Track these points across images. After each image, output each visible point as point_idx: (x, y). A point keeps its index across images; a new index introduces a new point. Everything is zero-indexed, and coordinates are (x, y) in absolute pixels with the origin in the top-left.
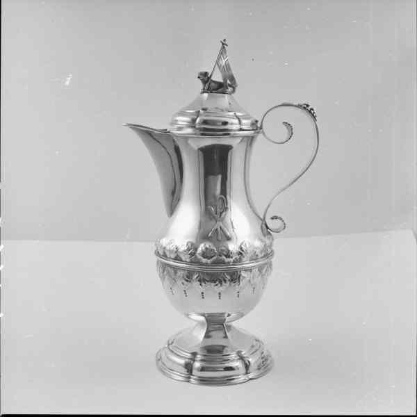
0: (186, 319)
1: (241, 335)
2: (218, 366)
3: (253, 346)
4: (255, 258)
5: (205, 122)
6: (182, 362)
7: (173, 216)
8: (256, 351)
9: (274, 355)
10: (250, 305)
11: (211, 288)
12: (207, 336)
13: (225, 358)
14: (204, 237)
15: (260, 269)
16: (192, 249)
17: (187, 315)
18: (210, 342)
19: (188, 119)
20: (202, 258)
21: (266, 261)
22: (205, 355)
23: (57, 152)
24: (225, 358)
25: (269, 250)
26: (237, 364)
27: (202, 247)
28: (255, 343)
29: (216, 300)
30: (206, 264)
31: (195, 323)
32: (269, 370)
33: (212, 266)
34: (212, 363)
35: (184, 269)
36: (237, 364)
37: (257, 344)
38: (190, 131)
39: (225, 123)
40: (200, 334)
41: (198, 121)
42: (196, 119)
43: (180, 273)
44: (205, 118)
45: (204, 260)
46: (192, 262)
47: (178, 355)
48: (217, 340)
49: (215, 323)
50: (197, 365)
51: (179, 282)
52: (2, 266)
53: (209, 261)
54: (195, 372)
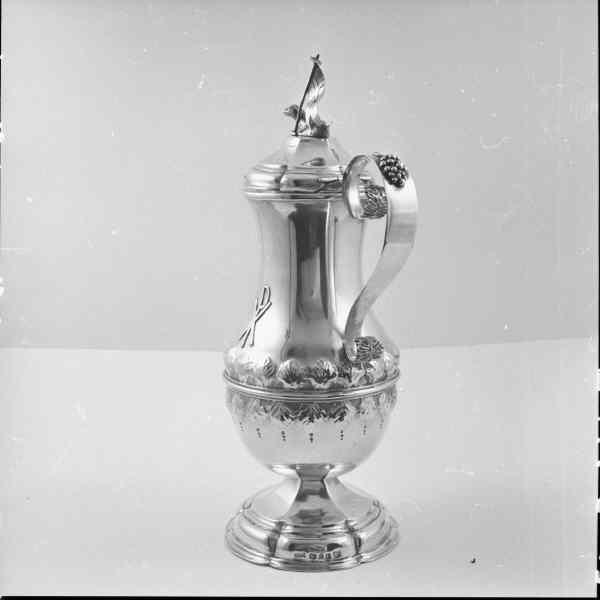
0: (268, 471)
1: (350, 498)
2: (311, 542)
3: (369, 513)
5: (297, 183)
6: (263, 535)
8: (373, 520)
9: (399, 519)
10: (365, 451)
11: (305, 427)
12: (301, 497)
13: (327, 530)
14: (291, 352)
15: (376, 396)
16: (270, 370)
18: (305, 506)
19: (272, 178)
20: (283, 381)
21: (384, 387)
22: (295, 527)
24: (327, 530)
26: (344, 540)
27: (284, 366)
28: (373, 507)
29: (317, 441)
30: (292, 391)
31: (282, 479)
32: (393, 547)
34: (309, 538)
35: (255, 397)
36: (344, 540)
37: (375, 510)
38: (273, 194)
40: (290, 495)
41: (283, 180)
42: (280, 178)
44: (298, 177)
45: (287, 385)
46: (271, 388)
48: (313, 504)
49: (312, 481)
50: (283, 540)
52: (598, 466)
54: (280, 552)
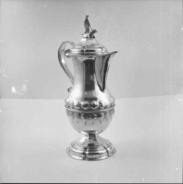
1: (101, 139)
4: (106, 107)
7: (70, 92)
10: (105, 127)
11: (91, 121)
15: (110, 111)
17: (80, 132)
23: (148, 43)
25: (113, 104)
29: (93, 125)
30: (85, 110)
33: (89, 111)
34: (91, 151)
39: (94, 51)
43: (82, 115)
44: (87, 49)
47: (75, 148)
49: (92, 135)
51: (75, 118)
53: (86, 109)
